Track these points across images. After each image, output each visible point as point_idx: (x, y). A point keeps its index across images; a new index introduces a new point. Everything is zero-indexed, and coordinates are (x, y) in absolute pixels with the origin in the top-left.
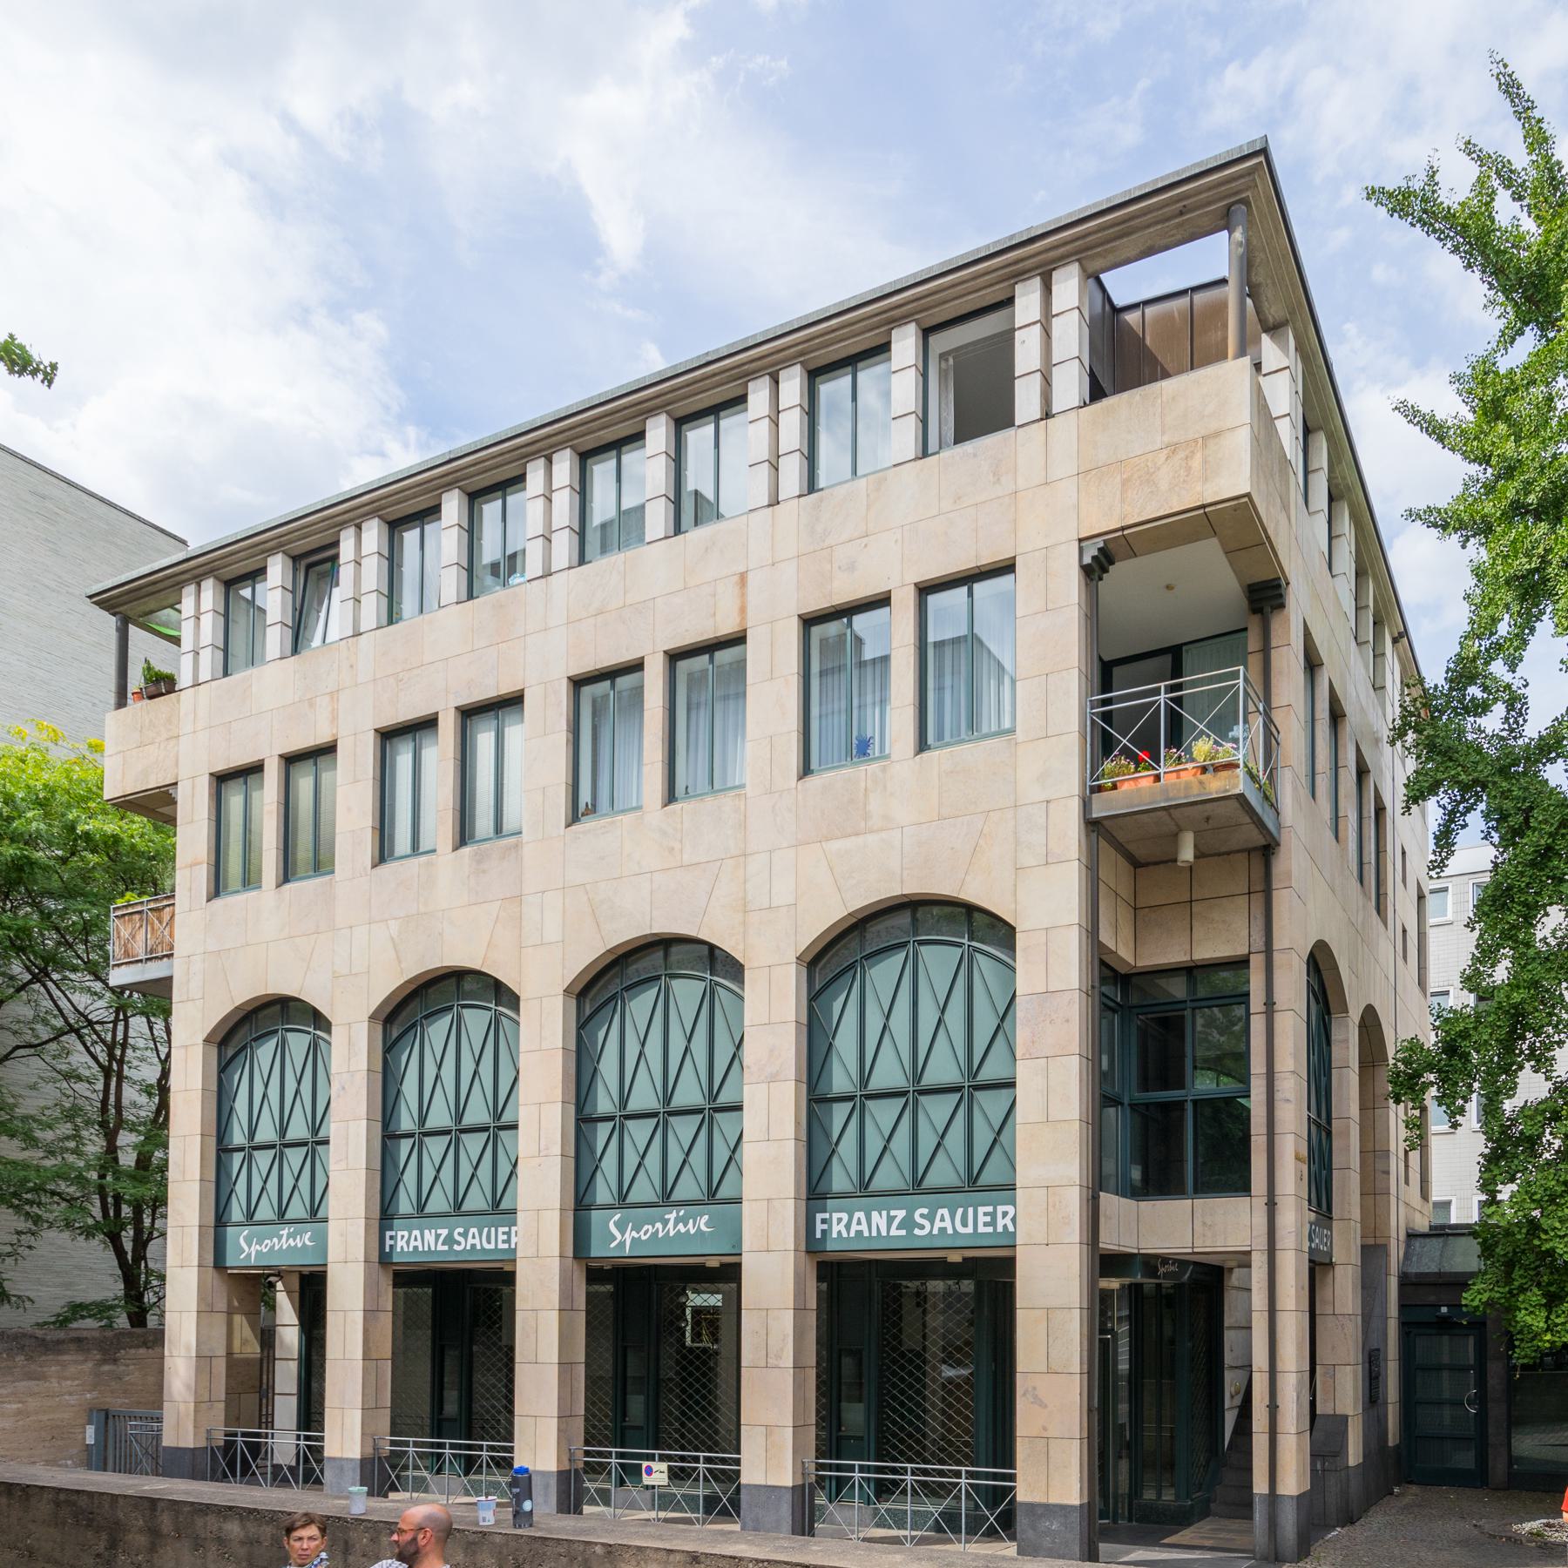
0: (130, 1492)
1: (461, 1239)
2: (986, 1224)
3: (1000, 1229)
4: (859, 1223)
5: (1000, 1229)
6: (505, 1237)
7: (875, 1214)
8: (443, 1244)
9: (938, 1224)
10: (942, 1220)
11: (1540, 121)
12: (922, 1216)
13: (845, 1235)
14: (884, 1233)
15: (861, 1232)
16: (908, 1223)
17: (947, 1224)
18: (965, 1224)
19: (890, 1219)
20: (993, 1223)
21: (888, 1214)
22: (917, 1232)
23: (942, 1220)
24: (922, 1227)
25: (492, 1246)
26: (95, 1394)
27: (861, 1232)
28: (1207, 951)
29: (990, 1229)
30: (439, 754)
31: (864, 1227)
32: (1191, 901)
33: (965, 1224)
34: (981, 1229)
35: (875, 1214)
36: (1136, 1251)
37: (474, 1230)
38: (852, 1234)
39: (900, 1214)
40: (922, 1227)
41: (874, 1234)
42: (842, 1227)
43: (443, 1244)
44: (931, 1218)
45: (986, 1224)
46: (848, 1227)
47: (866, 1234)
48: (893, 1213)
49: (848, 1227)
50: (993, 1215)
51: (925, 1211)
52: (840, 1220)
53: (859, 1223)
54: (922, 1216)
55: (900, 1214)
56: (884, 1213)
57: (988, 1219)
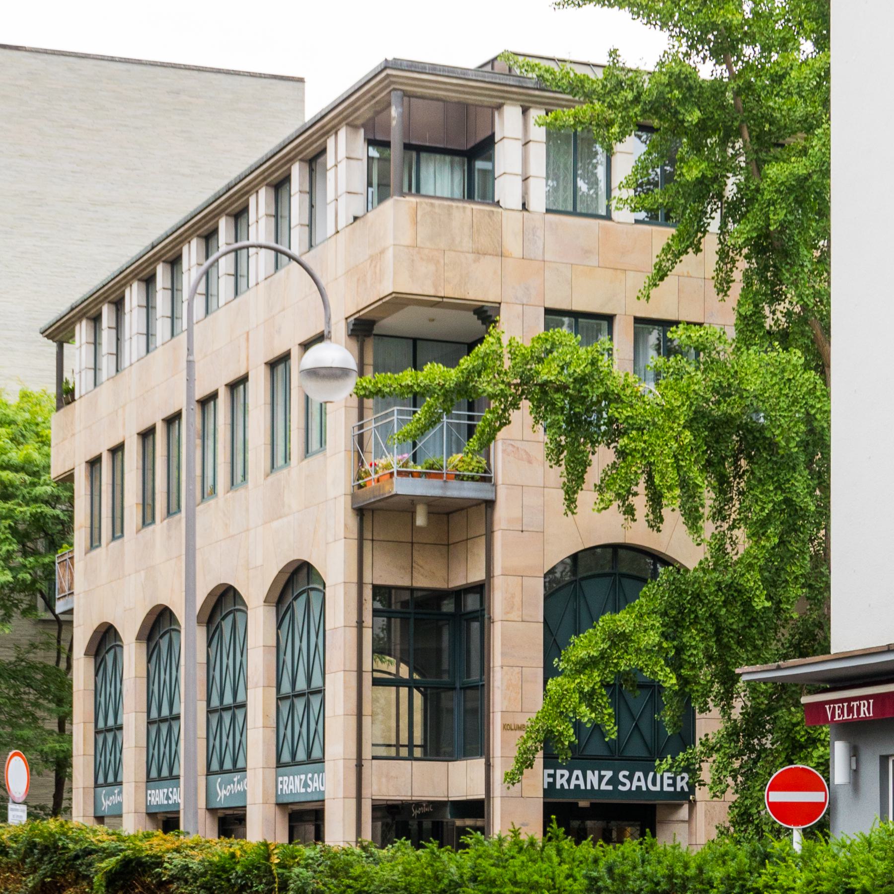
0: (133, 799)
1: (627, 781)
2: (669, 785)
3: (679, 789)
4: (577, 778)
5: (679, 789)
6: (671, 782)
7: (589, 773)
8: (607, 784)
9: (635, 783)
10: (639, 780)
11: (25, 396)
12: (624, 776)
13: (566, 787)
14: (596, 787)
15: (579, 785)
16: (614, 781)
17: (581, 782)
18: (654, 784)
19: (601, 778)
20: (674, 785)
21: (600, 773)
22: (620, 788)
23: (639, 780)
24: (624, 785)
25: (658, 788)
26: (496, 837)
27: (579, 785)
28: (458, 581)
29: (672, 789)
30: (321, 588)
31: (581, 782)
32: (448, 545)
33: (654, 784)
34: (666, 789)
35: (589, 773)
36: (446, 799)
37: (639, 774)
38: (572, 787)
39: (608, 774)
40: (624, 785)
41: (589, 787)
42: (564, 781)
43: (607, 784)
44: (630, 778)
45: (669, 785)
46: (569, 781)
47: (583, 787)
48: (603, 773)
49: (569, 781)
50: (674, 779)
51: (627, 773)
52: (562, 776)
53: (577, 778)
54: (624, 776)
55: (608, 774)
56: (596, 772)
57: (671, 782)
